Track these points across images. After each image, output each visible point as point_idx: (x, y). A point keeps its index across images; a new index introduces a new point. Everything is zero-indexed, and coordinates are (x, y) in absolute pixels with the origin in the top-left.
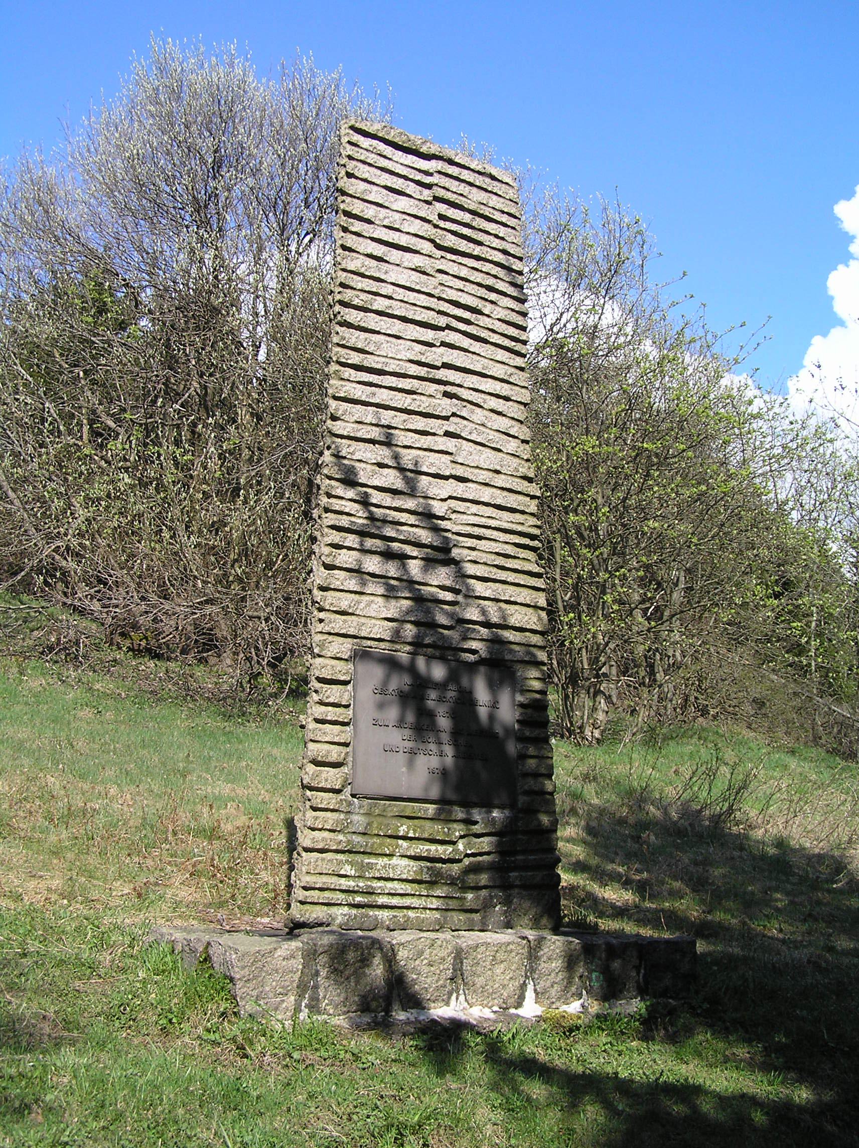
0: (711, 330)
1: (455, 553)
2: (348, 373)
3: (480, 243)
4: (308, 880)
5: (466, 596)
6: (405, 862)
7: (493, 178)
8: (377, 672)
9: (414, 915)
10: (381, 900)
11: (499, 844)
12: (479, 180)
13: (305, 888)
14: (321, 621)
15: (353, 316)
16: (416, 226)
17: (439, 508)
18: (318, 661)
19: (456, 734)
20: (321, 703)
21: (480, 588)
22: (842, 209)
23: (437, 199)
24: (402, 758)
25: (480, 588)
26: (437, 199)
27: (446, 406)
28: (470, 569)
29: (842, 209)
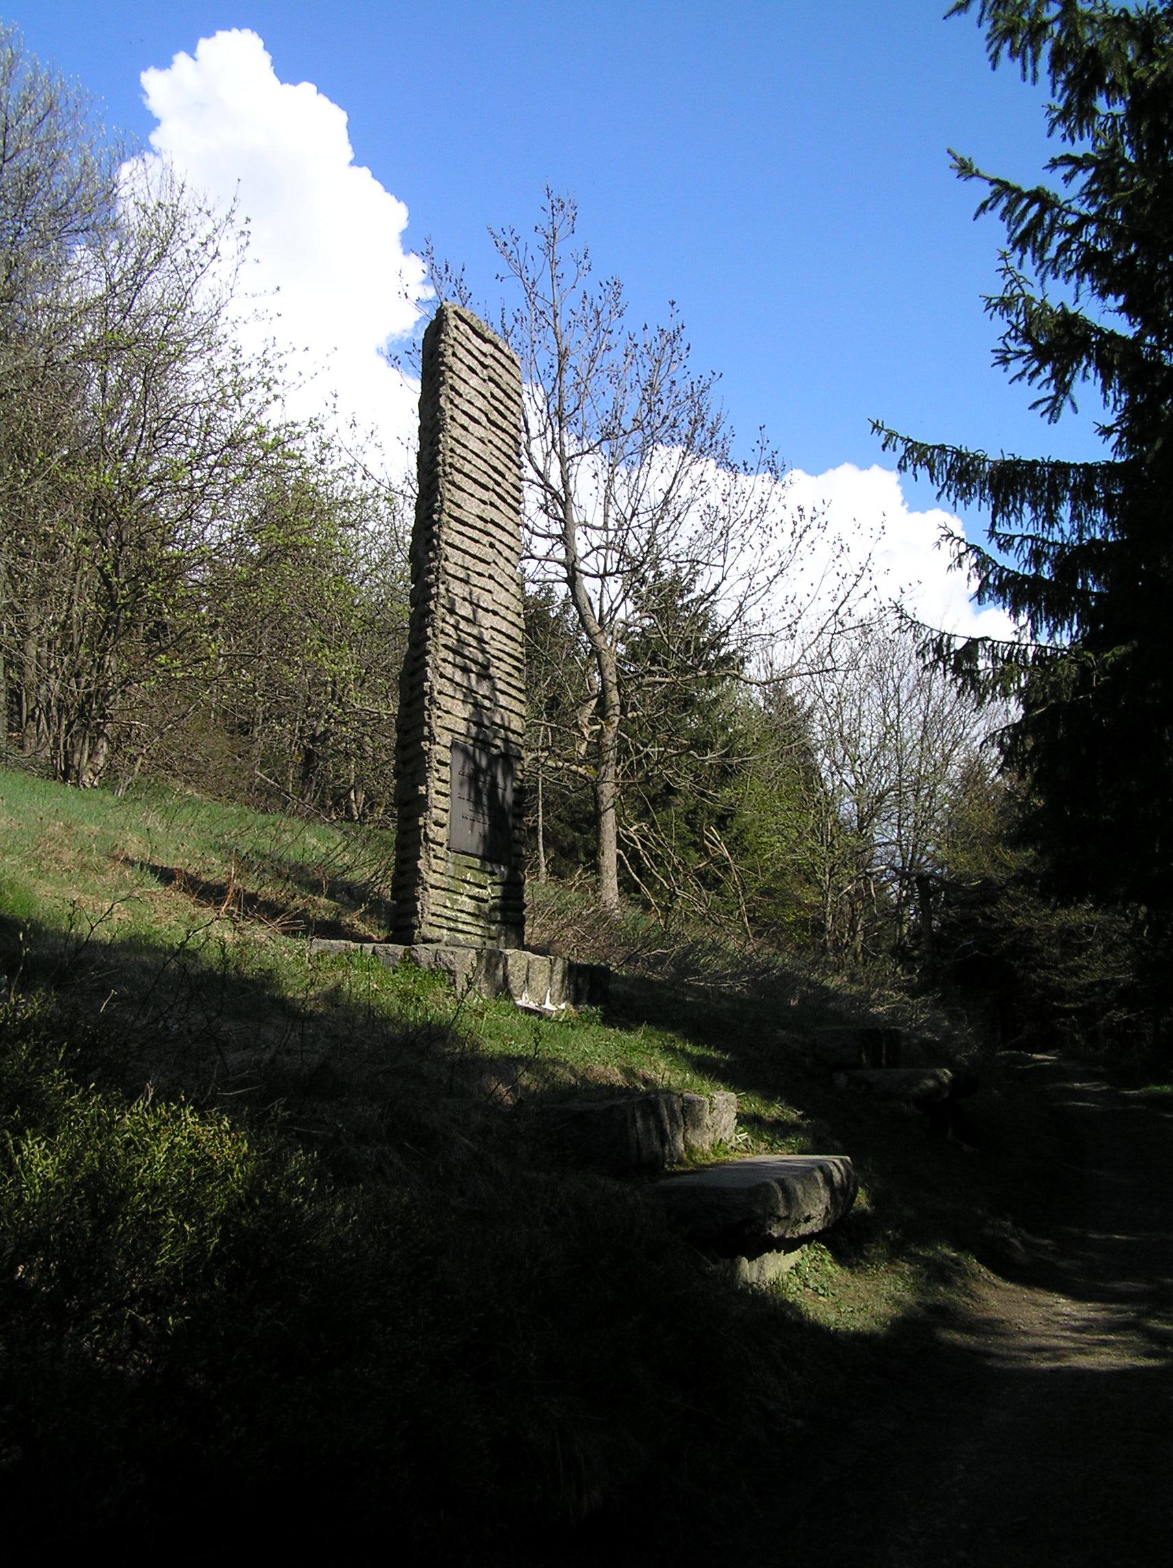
0: (1015, 627)
1: (492, 670)
2: (453, 524)
3: (505, 418)
4: (433, 909)
5: (496, 705)
6: (467, 900)
7: (513, 361)
8: (460, 758)
9: (931, 654)
10: (461, 926)
11: (504, 892)
12: (503, 360)
13: (433, 914)
14: (439, 717)
15: (458, 478)
16: (480, 402)
17: (487, 636)
18: (437, 747)
19: (489, 808)
20: (439, 780)
21: (503, 700)
22: (152, 80)
23: (491, 379)
24: (468, 822)
25: (503, 700)
26: (491, 379)
27: (489, 554)
28: (500, 685)
29: (152, 80)
